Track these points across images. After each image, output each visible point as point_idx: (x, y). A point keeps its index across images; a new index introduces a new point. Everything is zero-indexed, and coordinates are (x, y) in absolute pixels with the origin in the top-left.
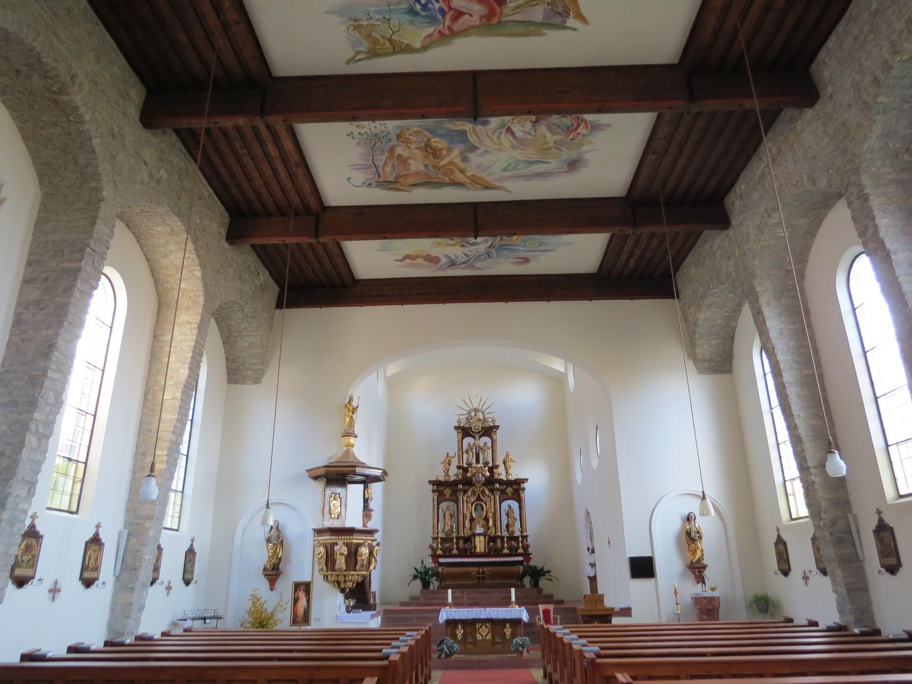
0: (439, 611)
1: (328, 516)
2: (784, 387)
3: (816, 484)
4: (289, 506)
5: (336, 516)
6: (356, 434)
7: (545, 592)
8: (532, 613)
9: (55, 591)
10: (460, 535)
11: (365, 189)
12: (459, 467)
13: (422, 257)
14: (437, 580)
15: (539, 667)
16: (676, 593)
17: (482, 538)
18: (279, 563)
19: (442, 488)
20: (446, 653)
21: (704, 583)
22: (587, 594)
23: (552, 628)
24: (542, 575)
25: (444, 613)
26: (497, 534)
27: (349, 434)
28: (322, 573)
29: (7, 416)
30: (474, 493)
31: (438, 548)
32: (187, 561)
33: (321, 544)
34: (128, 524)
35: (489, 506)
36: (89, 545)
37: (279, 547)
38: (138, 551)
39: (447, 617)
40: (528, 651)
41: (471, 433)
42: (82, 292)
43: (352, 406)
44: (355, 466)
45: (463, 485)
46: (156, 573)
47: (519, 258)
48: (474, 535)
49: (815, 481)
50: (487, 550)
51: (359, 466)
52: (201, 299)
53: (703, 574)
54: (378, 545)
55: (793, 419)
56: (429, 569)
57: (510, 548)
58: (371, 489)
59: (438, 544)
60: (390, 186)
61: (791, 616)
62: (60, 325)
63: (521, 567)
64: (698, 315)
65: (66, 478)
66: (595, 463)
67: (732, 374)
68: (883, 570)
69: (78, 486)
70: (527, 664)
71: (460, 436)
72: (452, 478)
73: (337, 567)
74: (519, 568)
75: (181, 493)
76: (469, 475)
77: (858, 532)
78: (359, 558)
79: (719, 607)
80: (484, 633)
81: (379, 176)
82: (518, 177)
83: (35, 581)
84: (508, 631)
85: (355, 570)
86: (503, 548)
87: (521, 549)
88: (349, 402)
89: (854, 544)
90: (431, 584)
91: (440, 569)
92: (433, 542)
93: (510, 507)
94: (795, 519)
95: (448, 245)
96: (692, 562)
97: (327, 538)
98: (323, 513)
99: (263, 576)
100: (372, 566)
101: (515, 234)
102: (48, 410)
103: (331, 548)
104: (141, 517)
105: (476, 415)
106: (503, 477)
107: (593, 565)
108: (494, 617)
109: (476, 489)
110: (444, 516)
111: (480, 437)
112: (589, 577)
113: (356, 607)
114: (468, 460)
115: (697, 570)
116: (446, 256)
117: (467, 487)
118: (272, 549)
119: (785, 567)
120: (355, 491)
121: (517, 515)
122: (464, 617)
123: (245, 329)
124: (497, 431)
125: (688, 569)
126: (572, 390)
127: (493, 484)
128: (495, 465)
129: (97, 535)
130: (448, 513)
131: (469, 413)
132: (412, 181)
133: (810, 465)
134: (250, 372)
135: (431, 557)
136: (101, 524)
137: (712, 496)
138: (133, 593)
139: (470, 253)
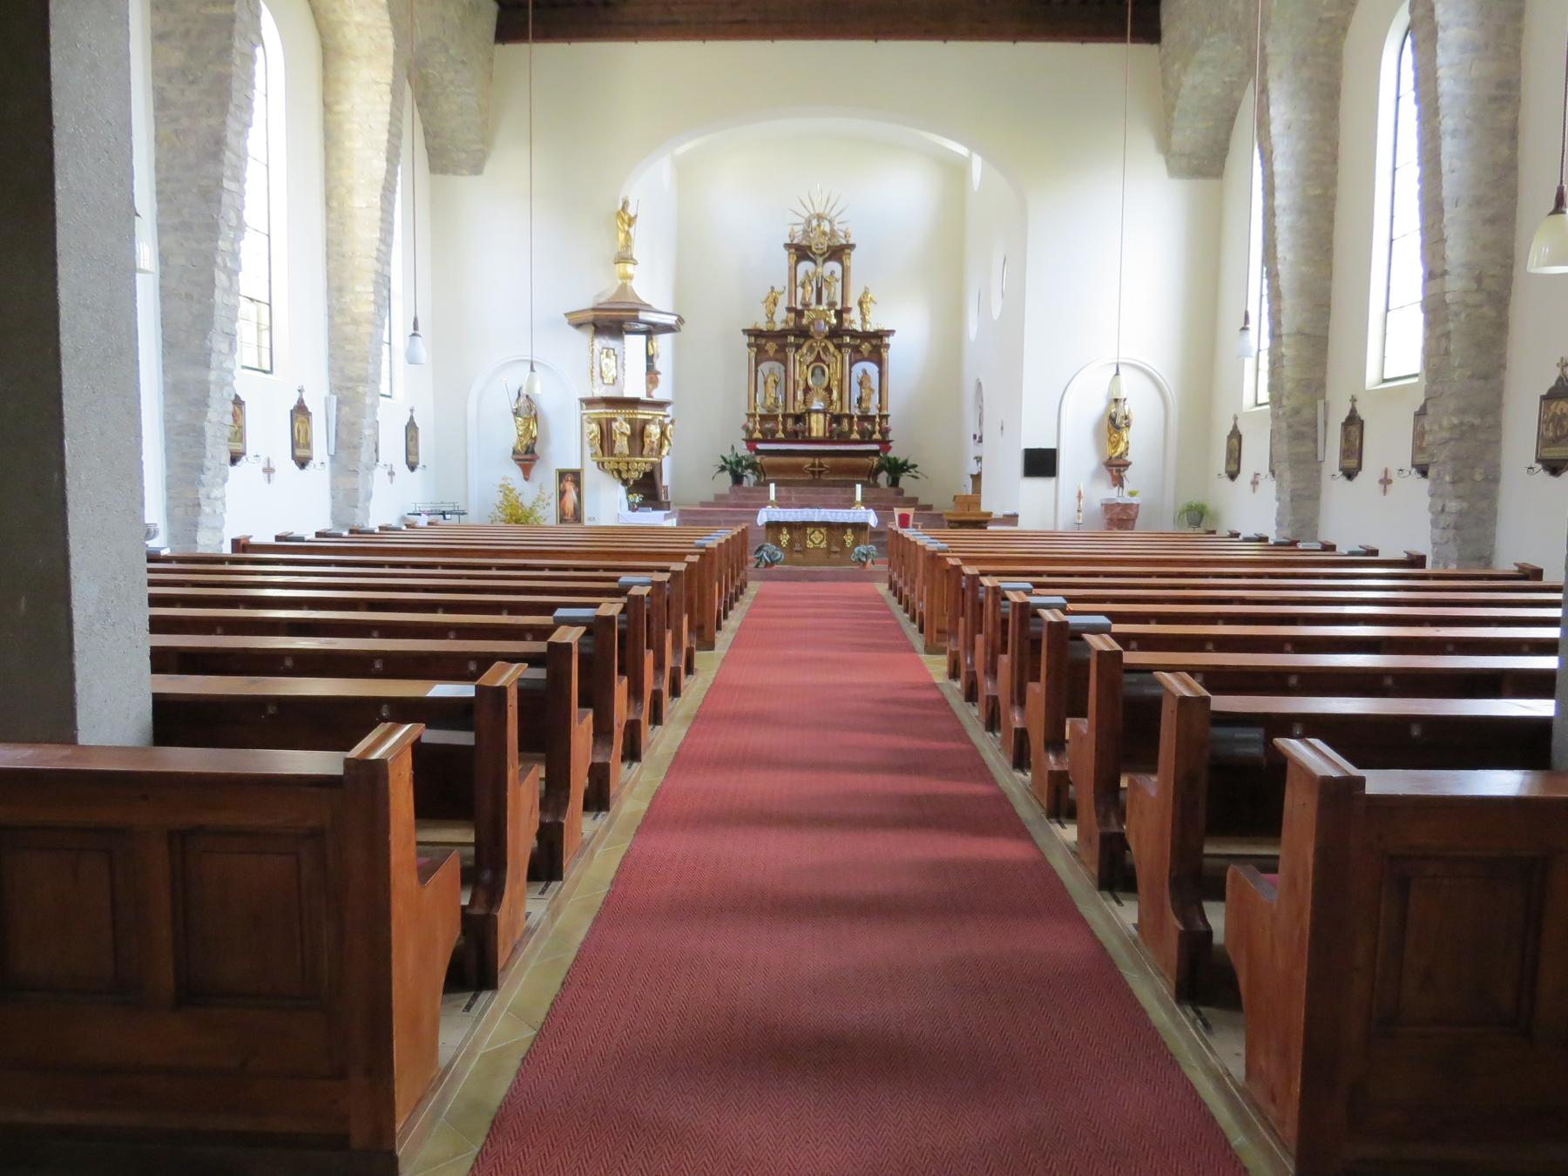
0: (756, 514)
1: (600, 380)
2: (1274, 215)
3: (1285, 359)
5: (611, 381)
7: (907, 494)
8: (882, 520)
10: (788, 412)
12: (790, 310)
14: (753, 474)
16: (1080, 496)
17: (821, 416)
18: (534, 444)
19: (763, 341)
20: (766, 561)
21: (1122, 485)
23: (908, 533)
24: (904, 471)
25: (765, 513)
26: (843, 412)
27: (624, 258)
28: (595, 458)
29: (182, 245)
30: (811, 349)
31: (755, 430)
34: (335, 388)
35: (833, 370)
36: (295, 415)
40: (873, 562)
41: (810, 255)
42: (243, 55)
43: (628, 214)
44: (637, 310)
45: (796, 336)
48: (809, 412)
49: (1285, 354)
50: (827, 434)
52: (390, 42)
53: (1122, 474)
54: (672, 422)
56: (743, 457)
57: (862, 432)
58: (657, 342)
59: (755, 424)
61: (1332, 541)
62: (224, 108)
66: (996, 314)
67: (1222, 178)
69: (266, 335)
70: (871, 578)
72: (779, 326)
73: (616, 451)
74: (872, 460)
76: (805, 321)
77: (1326, 424)
78: (647, 440)
79: (1136, 517)
80: (817, 539)
84: (849, 538)
85: (642, 456)
86: (851, 431)
87: (877, 433)
88: (623, 209)
89: (1316, 441)
90: (745, 478)
91: (758, 459)
92: (748, 421)
93: (865, 372)
94: (1261, 405)
96: (1111, 458)
97: (601, 412)
98: (592, 376)
99: (513, 461)
103: (607, 424)
104: (351, 379)
106: (858, 327)
107: (979, 459)
108: (831, 520)
109: (815, 344)
110: (765, 383)
111: (825, 261)
112: (972, 476)
113: (642, 505)
114: (804, 298)
115: (1116, 468)
117: (802, 341)
119: (1353, 463)
120: (634, 345)
122: (791, 520)
123: (452, 82)
125: (1104, 467)
127: (841, 336)
129: (301, 401)
130: (770, 380)
131: (809, 222)
134: (464, 156)
135: (744, 443)
137: (1154, 367)
138: (356, 477)
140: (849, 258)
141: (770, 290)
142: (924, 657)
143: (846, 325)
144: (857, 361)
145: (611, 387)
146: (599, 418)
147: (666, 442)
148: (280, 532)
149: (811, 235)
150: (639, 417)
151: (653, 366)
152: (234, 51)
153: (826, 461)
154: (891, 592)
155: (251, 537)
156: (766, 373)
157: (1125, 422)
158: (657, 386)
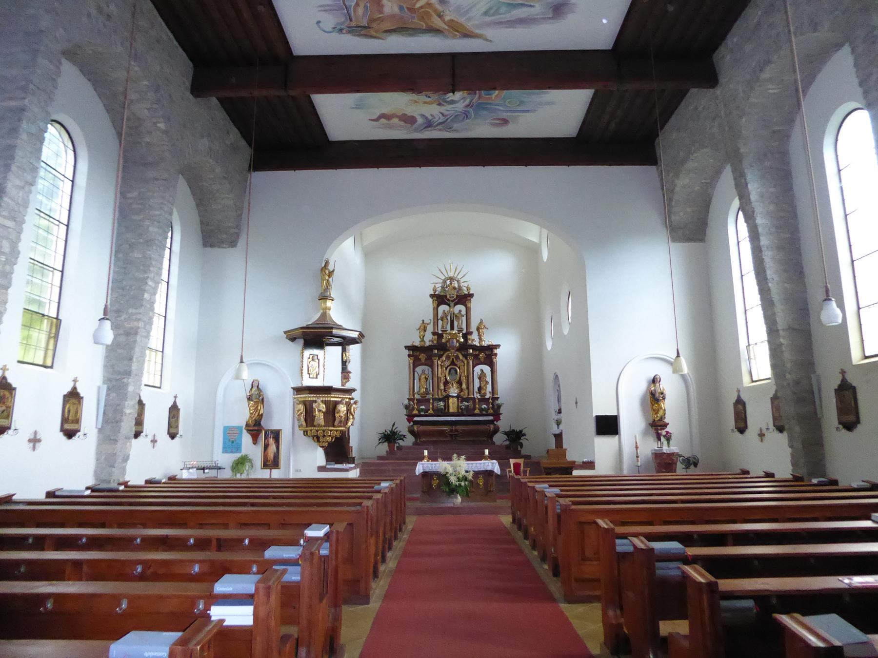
2: (761, 251)
4: (268, 365)
5: (315, 376)
6: (332, 298)
8: (504, 466)
9: (35, 441)
11: (335, 35)
12: (434, 334)
13: (397, 116)
15: (508, 514)
16: (637, 448)
17: (456, 399)
18: (261, 419)
22: (550, 448)
25: (421, 466)
30: (448, 357)
32: (171, 417)
33: (301, 402)
37: (260, 405)
38: (119, 405)
39: (423, 470)
44: (332, 328)
46: (140, 427)
47: (499, 119)
49: (783, 343)
51: (335, 328)
55: (767, 282)
58: (349, 352)
60: (362, 32)
61: (746, 468)
63: (492, 426)
64: (676, 181)
65: (29, 330)
66: (566, 331)
68: (841, 427)
71: (436, 303)
72: (428, 344)
73: (315, 423)
75: (161, 353)
76: (444, 340)
78: (337, 415)
81: (351, 20)
82: (501, 23)
83: (10, 432)
85: (334, 426)
86: (475, 408)
88: (325, 266)
93: (482, 370)
95: (425, 103)
100: (349, 422)
101: (495, 89)
102: (4, 259)
105: (451, 284)
111: (455, 305)
112: (555, 435)
114: (443, 327)
116: (423, 116)
118: (253, 406)
119: (742, 425)
120: (333, 353)
121: (489, 379)
123: (218, 190)
124: (472, 299)
126: (545, 260)
128: (468, 332)
129: (75, 388)
130: (423, 377)
131: (444, 282)
132: (387, 25)
133: (779, 328)
136: (78, 379)
139: (447, 113)
140: (470, 302)
141: (421, 322)
142: (564, 606)
143: (470, 342)
144: (478, 364)
145: (315, 379)
146: (303, 401)
147: (351, 417)
148: (148, 477)
149: (447, 289)
150: (332, 399)
151: (346, 368)
152: (21, 130)
153: (461, 428)
154: (515, 527)
155: (176, 476)
156: (420, 373)
157: (661, 396)
158: (348, 381)
